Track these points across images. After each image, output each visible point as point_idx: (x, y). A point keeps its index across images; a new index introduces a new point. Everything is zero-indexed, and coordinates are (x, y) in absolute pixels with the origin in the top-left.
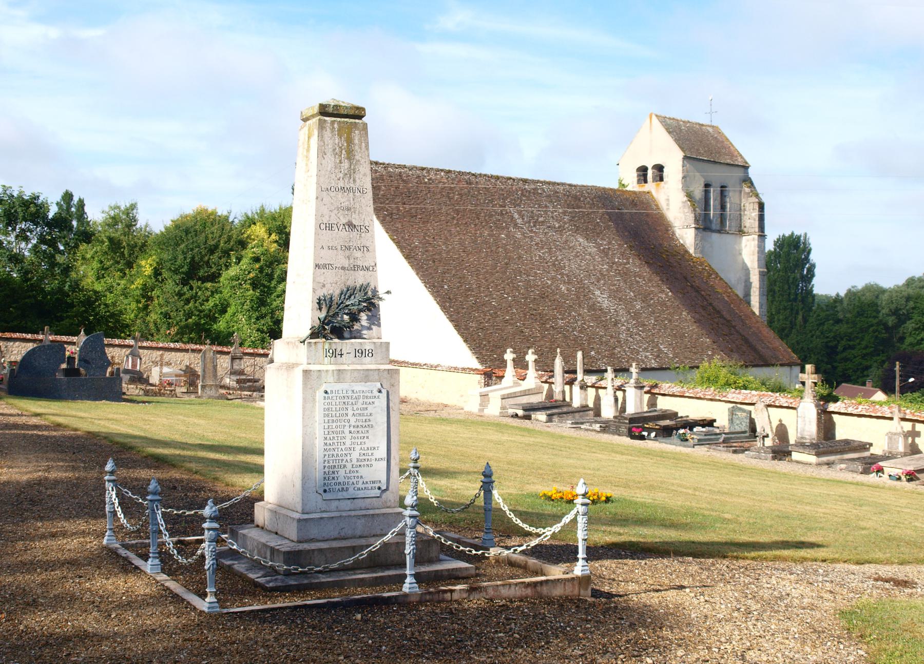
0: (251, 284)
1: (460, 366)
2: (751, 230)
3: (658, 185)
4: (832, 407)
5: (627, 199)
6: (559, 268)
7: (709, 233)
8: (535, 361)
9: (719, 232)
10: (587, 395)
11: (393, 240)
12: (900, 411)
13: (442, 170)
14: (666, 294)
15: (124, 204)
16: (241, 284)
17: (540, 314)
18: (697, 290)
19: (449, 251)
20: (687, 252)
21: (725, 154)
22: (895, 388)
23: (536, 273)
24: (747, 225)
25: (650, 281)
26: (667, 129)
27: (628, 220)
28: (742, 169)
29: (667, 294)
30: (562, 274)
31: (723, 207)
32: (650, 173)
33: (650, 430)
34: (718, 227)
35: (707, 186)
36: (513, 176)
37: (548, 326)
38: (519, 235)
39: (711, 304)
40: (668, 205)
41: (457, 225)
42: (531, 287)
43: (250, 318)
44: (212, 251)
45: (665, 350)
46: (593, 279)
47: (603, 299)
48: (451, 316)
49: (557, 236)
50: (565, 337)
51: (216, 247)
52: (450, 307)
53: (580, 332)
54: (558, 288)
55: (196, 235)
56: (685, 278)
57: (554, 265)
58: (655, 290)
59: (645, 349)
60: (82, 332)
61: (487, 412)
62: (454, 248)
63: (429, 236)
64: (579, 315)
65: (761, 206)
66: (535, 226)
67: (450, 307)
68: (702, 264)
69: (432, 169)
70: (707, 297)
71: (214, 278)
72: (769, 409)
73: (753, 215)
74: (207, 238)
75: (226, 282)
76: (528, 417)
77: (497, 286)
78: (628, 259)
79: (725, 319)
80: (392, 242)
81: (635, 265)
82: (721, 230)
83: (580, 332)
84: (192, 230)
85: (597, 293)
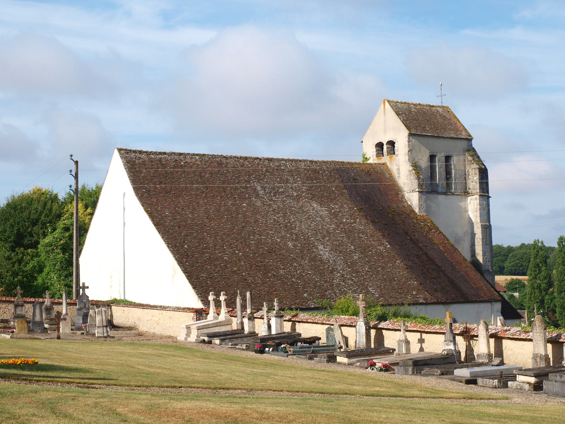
0: (61, 249)
1: (182, 306)
3: (391, 158)
4: (382, 325)
5: (363, 170)
6: (289, 228)
7: (436, 195)
8: (225, 300)
9: (445, 194)
10: (254, 324)
11: (147, 211)
12: (404, 324)
13: (197, 155)
14: (385, 246)
16: (53, 250)
17: (265, 265)
18: (415, 242)
20: (413, 211)
21: (451, 130)
22: (236, 305)
23: (268, 233)
24: (471, 187)
25: (372, 236)
26: (396, 112)
28: (466, 142)
29: (385, 247)
30: (292, 234)
31: (448, 173)
32: (385, 147)
33: (269, 346)
34: (444, 191)
35: (432, 158)
36: (260, 156)
37: (270, 275)
38: (259, 204)
39: (426, 254)
40: (399, 173)
41: (206, 197)
42: (261, 244)
43: (60, 276)
44: (34, 223)
45: (373, 292)
46: (319, 236)
47: (324, 252)
49: (293, 203)
50: (283, 283)
51: (37, 220)
52: (186, 262)
53: (298, 278)
54: (286, 244)
55: (22, 212)
56: (407, 233)
57: (286, 226)
58: (376, 243)
61: (189, 339)
62: (199, 216)
63: (179, 208)
64: (300, 265)
65: (483, 173)
67: (186, 262)
68: (425, 221)
69: (188, 154)
70: (424, 248)
71: (35, 245)
72: (342, 328)
73: (475, 178)
74: (30, 213)
75: (42, 248)
76: (210, 342)
77: (231, 244)
78: (355, 219)
79: (436, 265)
80: (145, 213)
81: (361, 224)
82: (447, 191)
83: (298, 278)
84: (19, 207)
85: (321, 247)
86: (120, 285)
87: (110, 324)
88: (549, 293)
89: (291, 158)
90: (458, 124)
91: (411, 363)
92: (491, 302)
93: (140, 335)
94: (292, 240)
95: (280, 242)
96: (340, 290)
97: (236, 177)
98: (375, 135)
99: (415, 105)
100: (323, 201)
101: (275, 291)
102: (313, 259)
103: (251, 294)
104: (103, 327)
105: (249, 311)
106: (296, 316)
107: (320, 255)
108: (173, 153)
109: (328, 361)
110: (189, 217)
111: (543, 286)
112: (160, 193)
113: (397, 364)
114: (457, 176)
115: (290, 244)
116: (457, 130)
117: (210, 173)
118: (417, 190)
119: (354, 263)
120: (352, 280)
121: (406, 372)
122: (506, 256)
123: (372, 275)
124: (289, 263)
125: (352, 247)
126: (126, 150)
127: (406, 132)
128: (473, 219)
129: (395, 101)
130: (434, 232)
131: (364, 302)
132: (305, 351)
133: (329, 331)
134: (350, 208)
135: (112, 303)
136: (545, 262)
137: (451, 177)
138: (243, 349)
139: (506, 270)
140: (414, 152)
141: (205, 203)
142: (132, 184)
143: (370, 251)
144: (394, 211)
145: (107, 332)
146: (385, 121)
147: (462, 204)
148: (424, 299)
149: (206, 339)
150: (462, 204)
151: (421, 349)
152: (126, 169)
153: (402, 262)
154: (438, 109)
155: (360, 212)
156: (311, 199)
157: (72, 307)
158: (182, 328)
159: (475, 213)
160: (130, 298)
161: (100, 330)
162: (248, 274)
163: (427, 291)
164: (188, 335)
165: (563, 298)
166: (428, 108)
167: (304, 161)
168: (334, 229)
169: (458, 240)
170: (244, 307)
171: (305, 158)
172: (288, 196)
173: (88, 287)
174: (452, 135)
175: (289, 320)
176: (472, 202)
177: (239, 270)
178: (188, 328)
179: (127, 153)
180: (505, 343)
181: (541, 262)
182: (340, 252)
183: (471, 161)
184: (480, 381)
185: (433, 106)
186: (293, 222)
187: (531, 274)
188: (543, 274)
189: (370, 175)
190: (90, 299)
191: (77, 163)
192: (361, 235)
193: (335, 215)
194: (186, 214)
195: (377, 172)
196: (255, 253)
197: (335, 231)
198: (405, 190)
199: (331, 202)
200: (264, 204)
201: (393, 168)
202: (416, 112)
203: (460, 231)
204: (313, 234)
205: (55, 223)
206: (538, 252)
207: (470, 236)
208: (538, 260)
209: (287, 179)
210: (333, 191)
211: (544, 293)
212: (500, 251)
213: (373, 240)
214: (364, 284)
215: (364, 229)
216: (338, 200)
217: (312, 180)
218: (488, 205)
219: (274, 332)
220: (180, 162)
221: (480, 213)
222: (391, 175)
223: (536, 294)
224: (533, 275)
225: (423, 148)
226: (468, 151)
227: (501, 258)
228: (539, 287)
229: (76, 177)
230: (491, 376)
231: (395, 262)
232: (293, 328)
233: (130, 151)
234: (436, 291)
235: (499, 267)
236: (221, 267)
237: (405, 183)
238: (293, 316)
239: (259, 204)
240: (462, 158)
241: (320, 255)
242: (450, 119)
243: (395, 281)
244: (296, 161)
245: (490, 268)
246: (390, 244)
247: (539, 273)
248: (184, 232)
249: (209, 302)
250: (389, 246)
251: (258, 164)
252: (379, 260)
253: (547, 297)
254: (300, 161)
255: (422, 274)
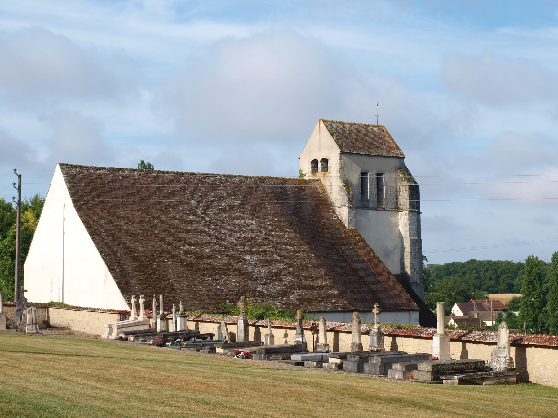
0: (10, 256)
1: (110, 308)
2: (405, 207)
3: (324, 174)
4: (260, 323)
6: (218, 239)
7: (366, 211)
8: (143, 302)
9: (376, 209)
11: (83, 222)
15: (33, 197)
16: (3, 256)
17: (192, 273)
19: (128, 229)
20: (343, 225)
21: (384, 148)
22: (152, 307)
23: (198, 244)
25: (299, 248)
26: (330, 131)
27: (296, 202)
28: (398, 160)
29: (311, 259)
31: (379, 189)
32: (319, 164)
33: (168, 341)
35: (364, 174)
36: (196, 172)
37: (196, 282)
38: (192, 216)
39: (350, 265)
40: (331, 189)
42: (190, 254)
45: (293, 299)
47: (250, 262)
48: (116, 275)
49: (225, 216)
50: (208, 290)
52: (117, 269)
54: (213, 254)
56: (334, 246)
57: (216, 238)
59: (276, 299)
60: (375, 311)
61: (111, 337)
62: (133, 227)
63: (114, 219)
65: (414, 191)
66: (207, 209)
67: (117, 269)
73: (405, 195)
76: (126, 339)
77: (161, 253)
78: (284, 232)
80: (82, 224)
81: (290, 238)
82: (378, 207)
86: (59, 289)
87: (47, 325)
88: (543, 311)
89: (226, 174)
90: (392, 143)
91: (263, 351)
92: (409, 311)
93: (71, 333)
94: (221, 250)
95: (209, 252)
96: (262, 297)
97: (171, 191)
98: (303, 154)
99: (349, 124)
100: (254, 214)
101: (199, 297)
102: (239, 269)
103: (163, 298)
104: (33, 324)
105: (161, 312)
106: (199, 316)
107: (246, 265)
108: (112, 168)
109: (210, 352)
110: (123, 228)
111: (537, 304)
112: (97, 205)
113: (254, 353)
114: (389, 193)
115: (218, 254)
116: (390, 149)
117: (146, 187)
118: (347, 205)
119: (278, 273)
120: (275, 288)
121: (260, 359)
122: (516, 273)
123: (294, 285)
124: (215, 271)
125: (279, 258)
126: (67, 165)
127: (337, 151)
128: (403, 234)
129: (330, 120)
130: (361, 245)
131: (243, 303)
132: (196, 345)
133: (219, 328)
134: (280, 222)
135: (49, 306)
136: (540, 279)
137: (382, 193)
138: (150, 344)
139: (515, 287)
140: (345, 169)
141: (140, 215)
142: (71, 197)
143: (295, 262)
144: (324, 225)
145: (36, 329)
146: (320, 140)
147: (393, 219)
148: (342, 308)
149: (123, 336)
150: (393, 219)
151: (286, 342)
152: (66, 182)
153: (325, 272)
154: (373, 128)
155: (290, 225)
156: (243, 213)
157: (12, 308)
158: (105, 327)
159: (405, 228)
160: (68, 301)
161: (30, 327)
162: (175, 281)
163: (346, 300)
164: (110, 333)
165: (557, 317)
166: (362, 127)
167: (239, 177)
168: (262, 241)
169: (387, 254)
170: (158, 307)
171: (240, 174)
172: (221, 209)
173: (26, 291)
174: (384, 154)
175: (193, 320)
176: (402, 217)
177: (167, 277)
178: (110, 327)
179: (69, 168)
180: (341, 335)
181: (535, 279)
182: (266, 262)
183: (402, 178)
184: (306, 363)
185: (368, 126)
186: (223, 234)
187: (524, 292)
188: (537, 291)
189: (304, 190)
190: (29, 301)
191: (20, 176)
192: (288, 247)
193: (265, 228)
194: (121, 226)
195: (310, 188)
196: (184, 262)
197: (263, 243)
198: (336, 205)
199: (263, 215)
200: (197, 217)
201: (326, 183)
202: (350, 132)
203: (390, 245)
204: (242, 245)
205: (6, 231)
206: (532, 268)
207: (400, 250)
208: (532, 277)
209: (221, 194)
210: (265, 205)
211: (537, 311)
212: (510, 268)
213: (300, 252)
214: (286, 292)
215: (292, 241)
216: (270, 214)
217: (246, 195)
218: (418, 221)
219: (178, 329)
220: (118, 177)
221: (409, 228)
222: (324, 191)
223: (529, 313)
224: (527, 292)
225: (355, 166)
226: (400, 168)
227: (511, 275)
228: (532, 305)
229: (19, 190)
230: (313, 359)
231: (319, 273)
232: (197, 327)
233: (71, 166)
234: (356, 300)
235: (508, 284)
236: (150, 274)
237: (336, 199)
238: (197, 317)
239: (192, 216)
240: (393, 175)
241: (246, 265)
242: (384, 138)
243: (316, 290)
244: (231, 177)
245: (418, 280)
246: (315, 256)
247: (533, 291)
248: (118, 242)
249: (140, 304)
250: (314, 258)
251: (194, 179)
252: (303, 270)
253: (541, 315)
254: (235, 177)
255: (344, 284)
